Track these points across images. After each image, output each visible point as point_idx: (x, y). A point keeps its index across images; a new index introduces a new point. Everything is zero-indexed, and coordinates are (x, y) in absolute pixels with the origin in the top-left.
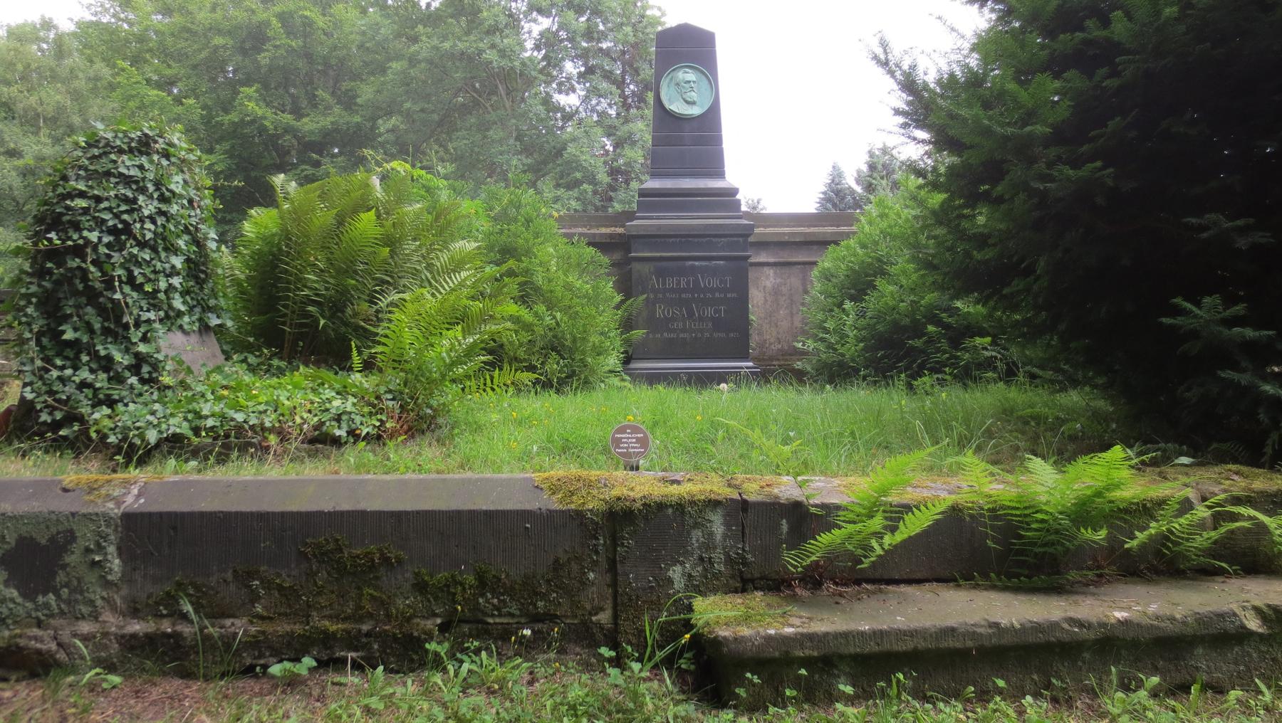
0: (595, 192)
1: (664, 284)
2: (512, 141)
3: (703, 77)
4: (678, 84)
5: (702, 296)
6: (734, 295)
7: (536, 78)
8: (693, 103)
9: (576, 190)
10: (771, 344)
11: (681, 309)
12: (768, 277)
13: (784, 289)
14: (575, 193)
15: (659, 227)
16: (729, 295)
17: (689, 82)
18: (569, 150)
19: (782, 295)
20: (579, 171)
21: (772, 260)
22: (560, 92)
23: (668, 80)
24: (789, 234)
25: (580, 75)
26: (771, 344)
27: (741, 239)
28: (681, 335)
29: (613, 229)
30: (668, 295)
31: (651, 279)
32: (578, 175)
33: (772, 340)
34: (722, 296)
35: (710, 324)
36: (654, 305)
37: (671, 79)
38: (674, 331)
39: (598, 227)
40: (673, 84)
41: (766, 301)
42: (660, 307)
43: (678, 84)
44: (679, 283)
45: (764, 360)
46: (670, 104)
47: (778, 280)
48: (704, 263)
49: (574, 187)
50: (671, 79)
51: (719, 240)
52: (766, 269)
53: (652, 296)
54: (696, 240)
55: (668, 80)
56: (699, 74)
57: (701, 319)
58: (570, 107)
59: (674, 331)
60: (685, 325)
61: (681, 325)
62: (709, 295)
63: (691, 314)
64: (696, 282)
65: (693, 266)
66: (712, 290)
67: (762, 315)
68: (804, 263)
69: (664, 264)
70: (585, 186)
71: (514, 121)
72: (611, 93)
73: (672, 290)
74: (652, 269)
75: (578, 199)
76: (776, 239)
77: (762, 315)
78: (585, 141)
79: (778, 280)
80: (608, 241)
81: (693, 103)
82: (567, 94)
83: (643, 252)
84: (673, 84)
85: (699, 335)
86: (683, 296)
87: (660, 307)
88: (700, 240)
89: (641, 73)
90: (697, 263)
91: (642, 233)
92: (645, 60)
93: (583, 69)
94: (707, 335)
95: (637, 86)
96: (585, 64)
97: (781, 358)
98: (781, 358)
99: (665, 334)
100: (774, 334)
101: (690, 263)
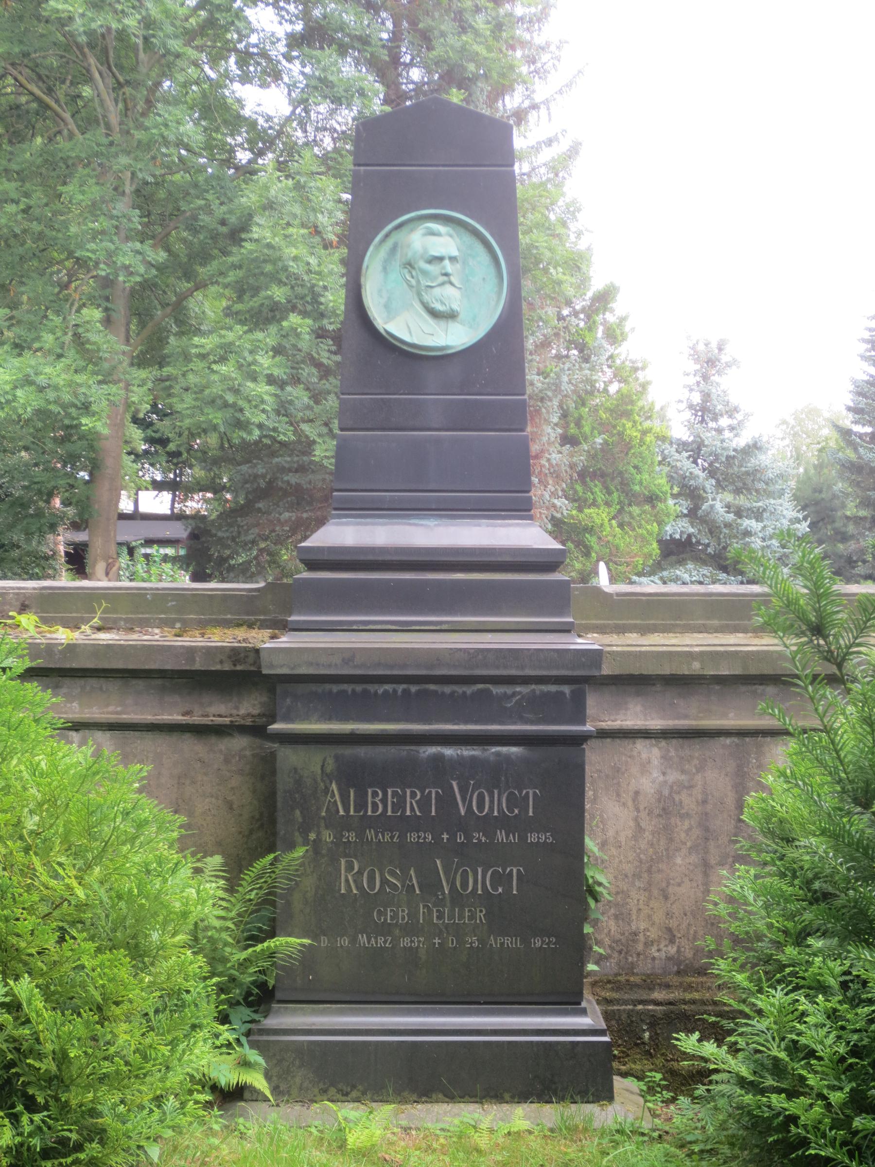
0: (320, 334)
1: (361, 805)
2: (121, 207)
3: (479, 248)
4: (409, 265)
5: (460, 838)
6: (545, 837)
7: (178, 56)
8: (451, 316)
9: (273, 329)
10: (648, 944)
11: (405, 876)
12: (644, 768)
13: (688, 801)
14: (268, 337)
15: (349, 655)
16: (532, 838)
17: (441, 259)
18: (256, 232)
19: (683, 817)
20: (280, 283)
21: (656, 723)
22: (245, 79)
23: (383, 253)
24: (701, 656)
25: (295, 41)
26: (648, 944)
27: (566, 689)
28: (405, 942)
29: (241, 633)
30: (370, 834)
31: (327, 790)
32: (278, 293)
33: (653, 934)
34: (514, 839)
35: (481, 915)
36: (334, 861)
37: (394, 249)
38: (384, 930)
39: (203, 625)
40: (396, 265)
41: (639, 829)
42: (350, 868)
43: (409, 265)
44: (400, 805)
45: (632, 986)
46: (389, 319)
47: (673, 776)
48: (467, 752)
49: (268, 321)
50: (394, 249)
51: (508, 690)
52: (640, 745)
53: (328, 836)
54: (447, 689)
55: (383, 253)
56: (468, 239)
57: (457, 899)
58: (269, 119)
59: (384, 930)
60: (413, 915)
61: (404, 913)
62: (478, 837)
63: (431, 886)
64: (447, 802)
65: (438, 759)
66: (488, 824)
67: (628, 868)
68: (742, 733)
69: (362, 751)
70: (294, 319)
71: (124, 160)
72: (362, 93)
73: (382, 823)
74: (331, 766)
75: (278, 351)
76: (666, 670)
77: (628, 868)
78: (297, 209)
79: (673, 776)
80: (227, 667)
81: (451, 316)
82: (264, 85)
83: (306, 718)
84: (396, 265)
85: (452, 942)
86: (412, 837)
87: (350, 868)
88: (459, 689)
89: (437, 43)
90: (449, 752)
91: (303, 670)
92: (448, 10)
93: (299, 27)
94: (473, 941)
95: (429, 72)
96: (306, 16)
97: (675, 980)
98: (675, 980)
99: (363, 939)
100: (659, 917)
101: (432, 750)
